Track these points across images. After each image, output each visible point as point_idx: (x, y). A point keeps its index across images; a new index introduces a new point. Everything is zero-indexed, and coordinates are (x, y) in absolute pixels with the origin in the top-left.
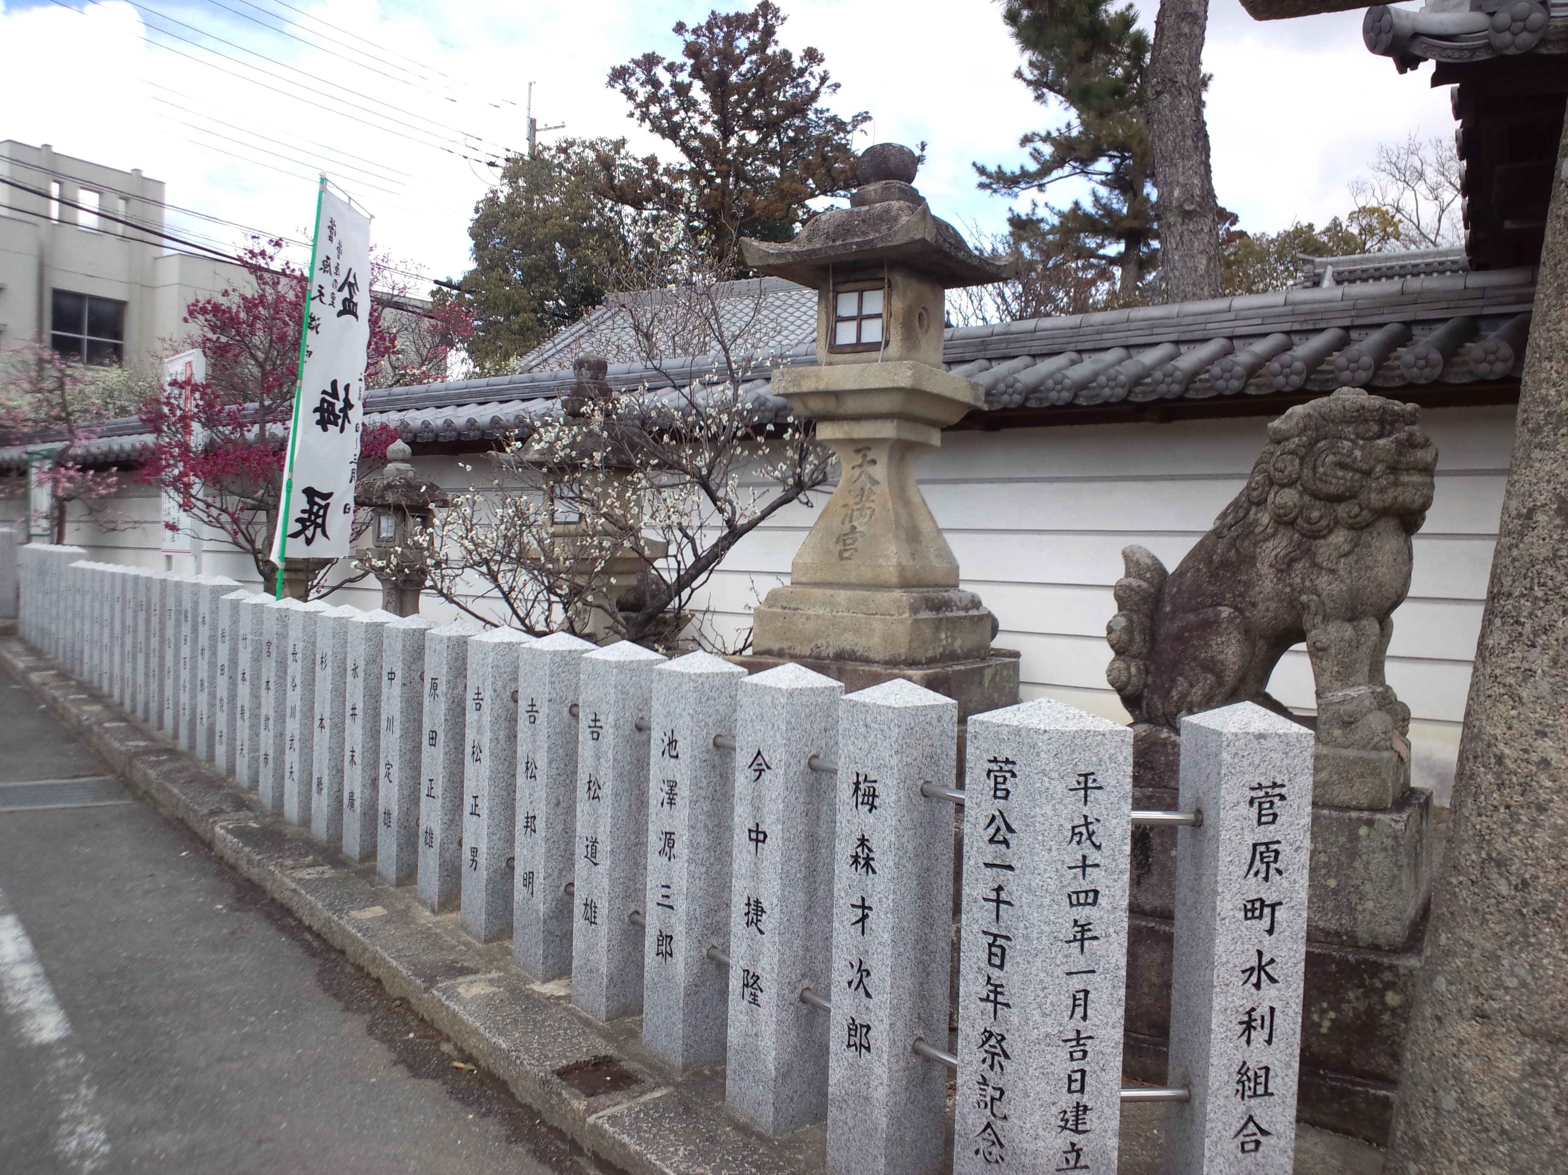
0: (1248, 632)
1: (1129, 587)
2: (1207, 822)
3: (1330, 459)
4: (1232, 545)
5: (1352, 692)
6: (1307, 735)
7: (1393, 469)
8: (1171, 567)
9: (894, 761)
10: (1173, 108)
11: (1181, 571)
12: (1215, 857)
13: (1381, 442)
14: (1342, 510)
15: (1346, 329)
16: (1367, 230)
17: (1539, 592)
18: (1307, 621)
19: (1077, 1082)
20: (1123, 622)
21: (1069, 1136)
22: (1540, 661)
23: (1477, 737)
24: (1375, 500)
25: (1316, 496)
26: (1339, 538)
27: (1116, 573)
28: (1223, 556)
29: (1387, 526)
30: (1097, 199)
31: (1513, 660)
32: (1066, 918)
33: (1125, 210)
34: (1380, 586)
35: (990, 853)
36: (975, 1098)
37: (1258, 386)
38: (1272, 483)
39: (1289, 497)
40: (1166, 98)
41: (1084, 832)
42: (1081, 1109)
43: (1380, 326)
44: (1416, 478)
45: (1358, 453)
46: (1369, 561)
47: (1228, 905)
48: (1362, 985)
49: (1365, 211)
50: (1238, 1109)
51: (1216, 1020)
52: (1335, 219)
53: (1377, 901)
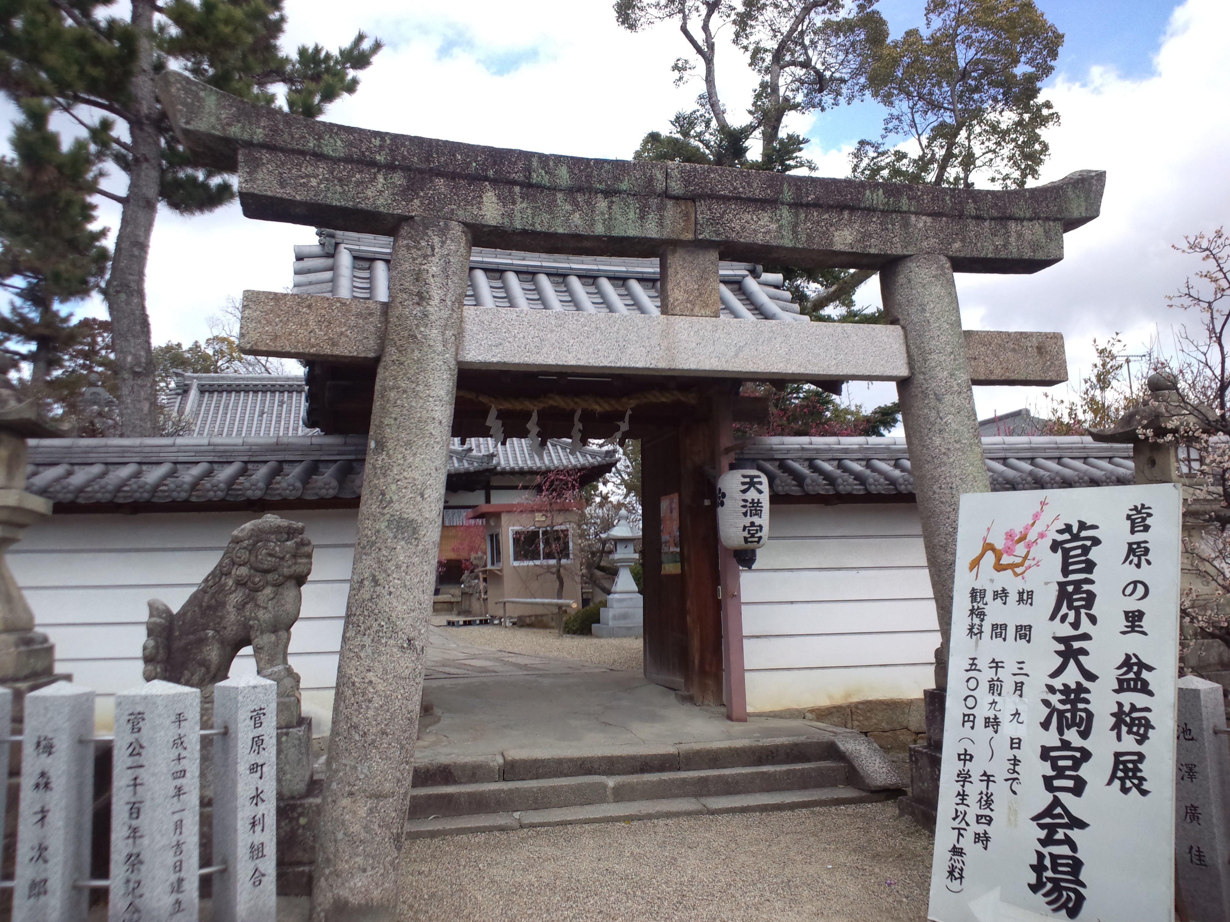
0: (222, 642)
1: (155, 623)
2: (230, 731)
3: (264, 551)
4: (213, 596)
5: (276, 669)
6: (271, 685)
7: (294, 556)
8: (175, 610)
9: (67, 725)
10: (128, 303)
11: (178, 613)
12: (236, 746)
13: (288, 543)
14: (270, 577)
15: (246, 462)
16: (220, 353)
17: (366, 613)
18: (253, 634)
19: (178, 867)
20: (152, 643)
21: (174, 896)
22: (367, 641)
23: (344, 676)
24: (286, 571)
25: (257, 570)
26: (268, 591)
27: (144, 616)
28: (207, 602)
29: (291, 584)
30: (14, 309)
31: (357, 642)
32: (170, 786)
33: (38, 320)
34: (288, 614)
35: (130, 762)
36: (122, 892)
37: (198, 496)
38: (234, 564)
39: (243, 571)
40: (123, 296)
41: (179, 742)
42: (180, 881)
43: (266, 462)
44: (304, 560)
45: (277, 549)
46: (283, 602)
47: (243, 768)
48: (287, 817)
49: (216, 338)
50: (251, 866)
51: (240, 824)
52: (196, 342)
53: (292, 773)
